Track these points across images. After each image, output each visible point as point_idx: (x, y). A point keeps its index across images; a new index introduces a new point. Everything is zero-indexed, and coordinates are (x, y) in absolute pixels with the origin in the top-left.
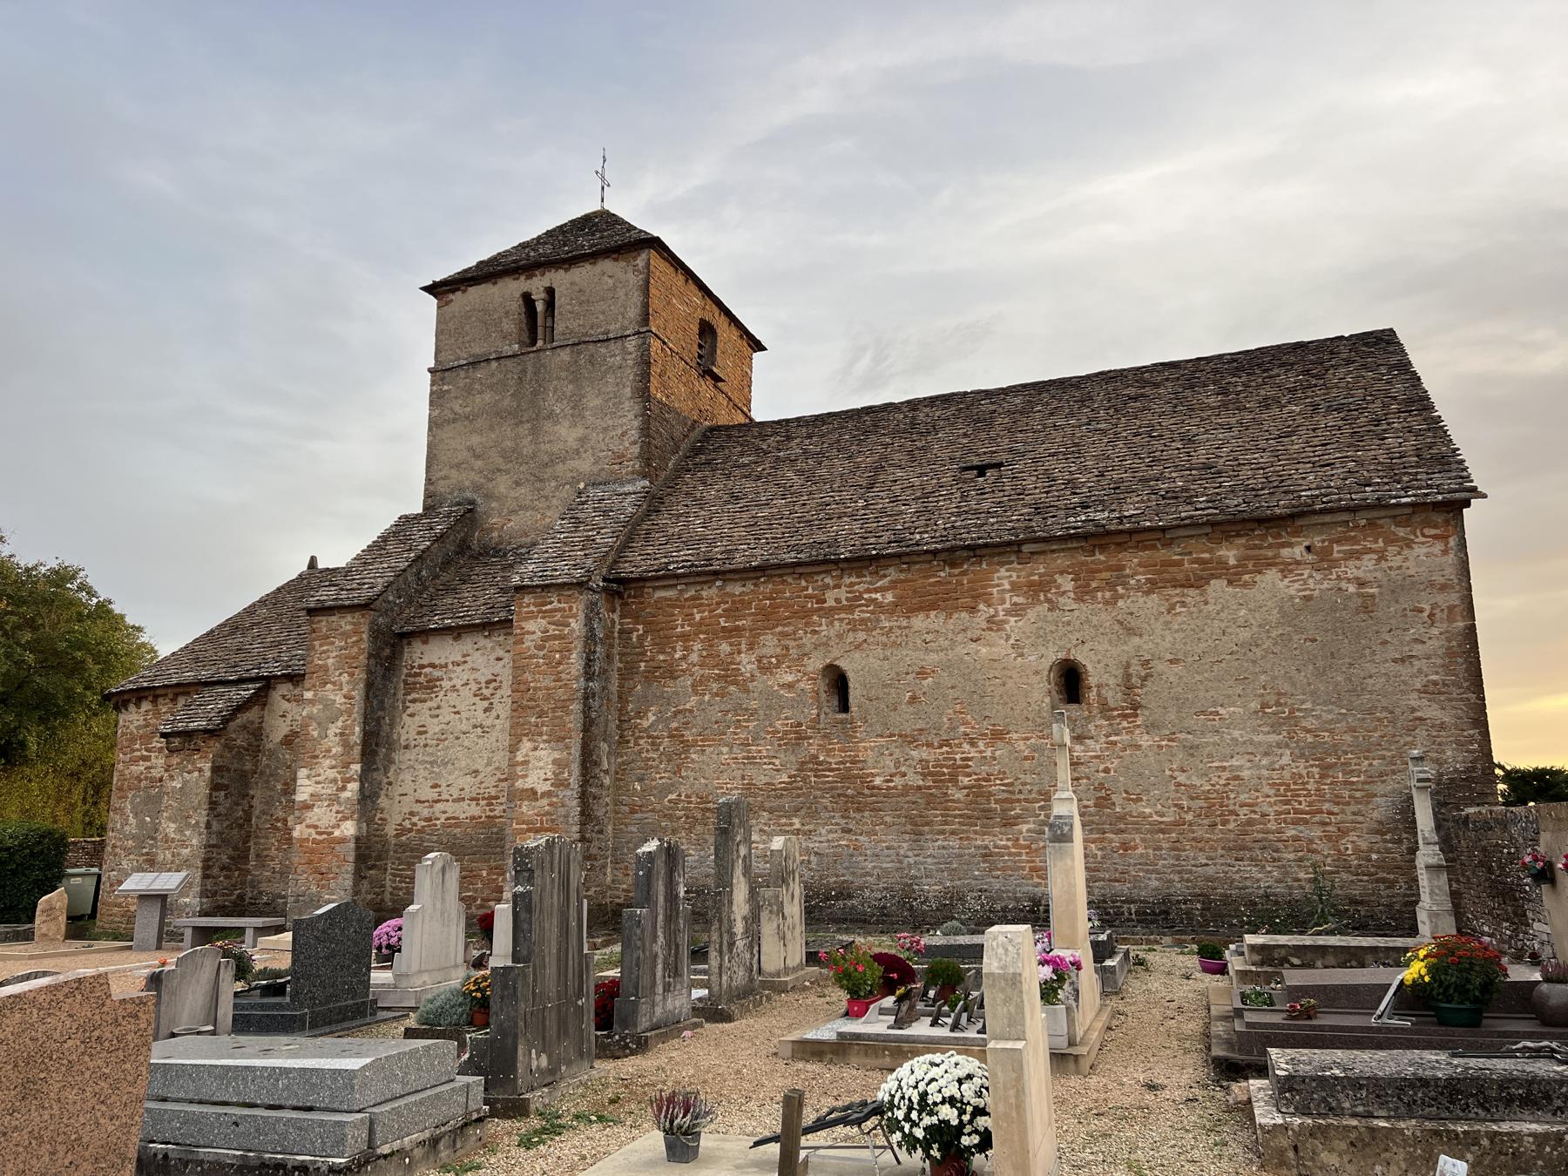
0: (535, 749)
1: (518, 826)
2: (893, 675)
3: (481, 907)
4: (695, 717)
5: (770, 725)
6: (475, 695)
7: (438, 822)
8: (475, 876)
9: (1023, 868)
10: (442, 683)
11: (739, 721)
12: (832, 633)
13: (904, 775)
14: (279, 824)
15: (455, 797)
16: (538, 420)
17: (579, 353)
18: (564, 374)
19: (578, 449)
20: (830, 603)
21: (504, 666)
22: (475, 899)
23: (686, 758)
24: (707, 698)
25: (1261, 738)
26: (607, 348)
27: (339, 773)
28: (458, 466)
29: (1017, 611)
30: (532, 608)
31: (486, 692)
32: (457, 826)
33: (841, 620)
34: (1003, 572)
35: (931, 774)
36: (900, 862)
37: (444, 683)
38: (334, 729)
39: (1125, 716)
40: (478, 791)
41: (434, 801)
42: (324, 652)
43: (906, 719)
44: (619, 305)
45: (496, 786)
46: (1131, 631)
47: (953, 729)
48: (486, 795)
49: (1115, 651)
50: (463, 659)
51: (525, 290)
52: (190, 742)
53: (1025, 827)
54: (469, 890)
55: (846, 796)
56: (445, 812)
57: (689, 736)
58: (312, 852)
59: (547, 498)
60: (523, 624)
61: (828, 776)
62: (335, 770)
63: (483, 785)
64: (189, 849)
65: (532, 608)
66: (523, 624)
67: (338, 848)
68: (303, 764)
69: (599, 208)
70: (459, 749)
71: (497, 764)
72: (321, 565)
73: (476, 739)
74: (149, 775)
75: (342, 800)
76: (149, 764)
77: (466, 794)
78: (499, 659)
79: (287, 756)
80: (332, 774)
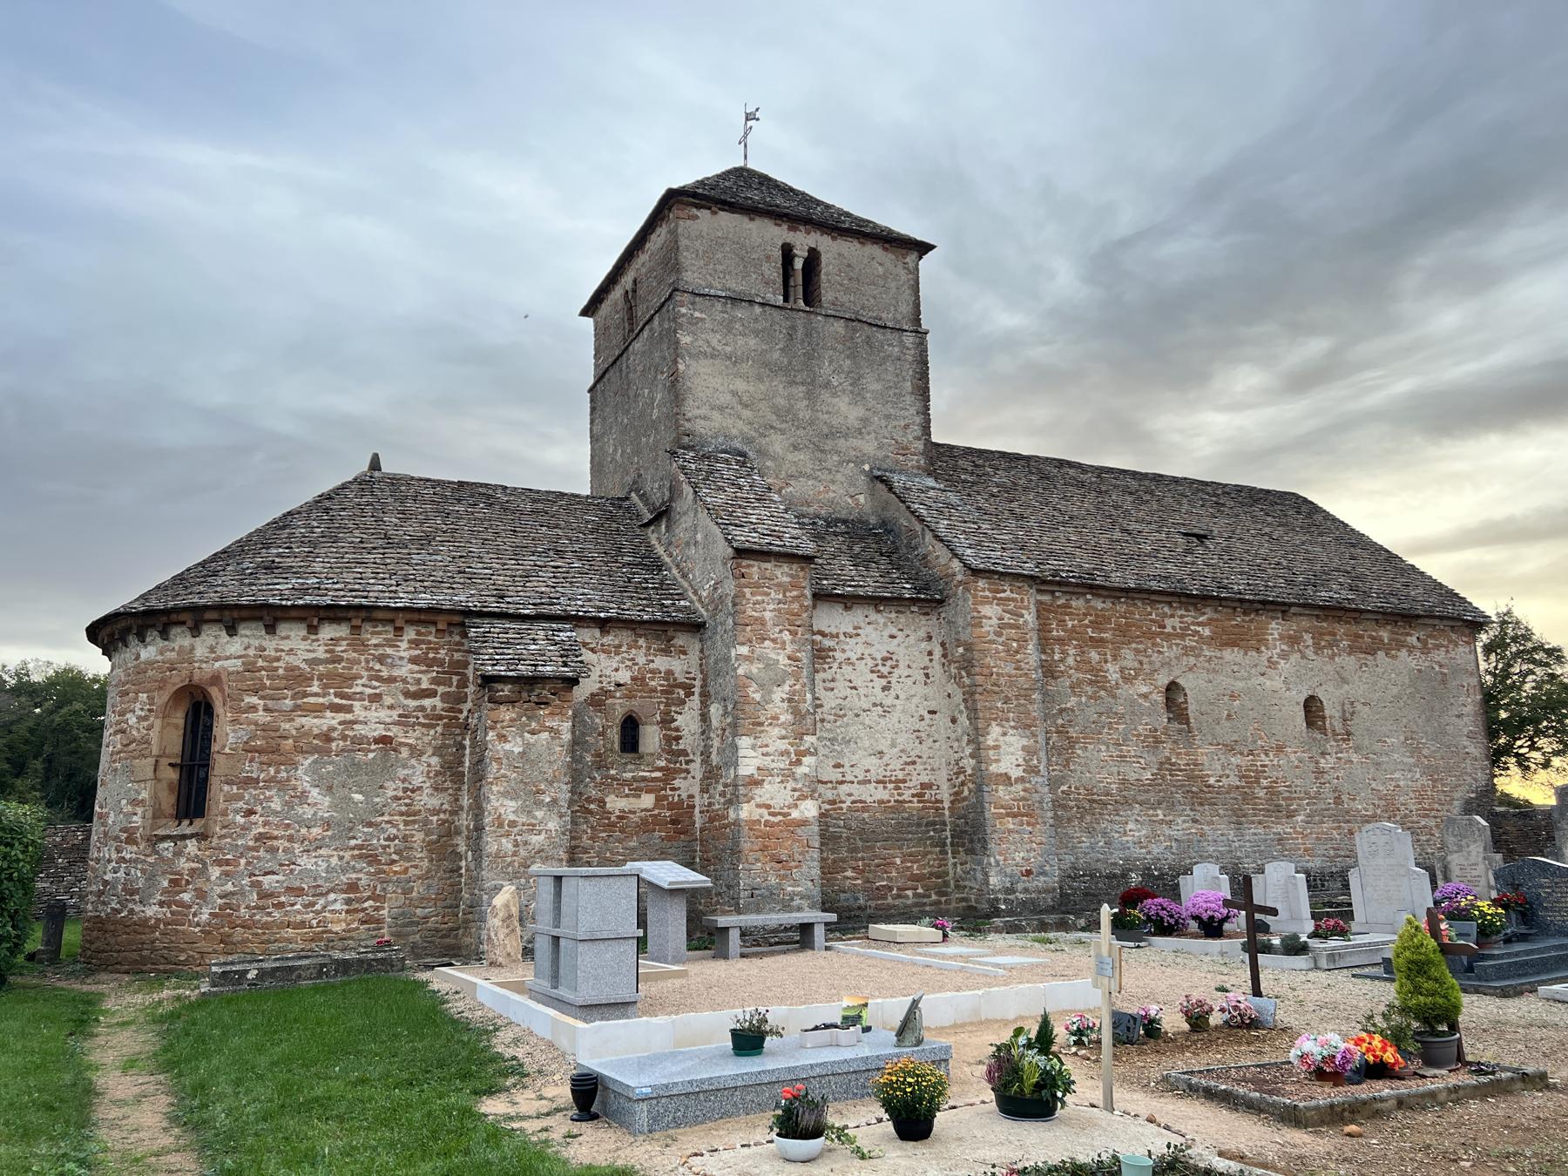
0: (1005, 734)
1: (997, 811)
2: (1215, 696)
3: (899, 896)
4: (1076, 716)
5: (1135, 729)
6: (872, 672)
7: (844, 806)
8: (888, 864)
9: (1300, 849)
10: (835, 654)
11: (1111, 723)
12: (1172, 655)
13: (1228, 776)
14: (592, 806)
15: (860, 778)
16: (814, 387)
17: (855, 330)
18: (840, 347)
19: (860, 429)
20: (1169, 630)
21: (899, 645)
22: (891, 889)
23: (1073, 753)
24: (1084, 699)
25: (1405, 760)
26: (884, 334)
27: (791, 744)
28: (721, 409)
29: (1284, 656)
30: (987, 593)
31: (885, 670)
32: (864, 810)
33: (1177, 645)
34: (1273, 625)
35: (1244, 776)
36: (1230, 846)
37: (838, 655)
38: (779, 694)
39: (1344, 740)
40: (885, 773)
41: (837, 782)
42: (757, 603)
43: (1225, 732)
44: (890, 296)
45: (903, 770)
46: (1344, 681)
47: (1255, 742)
48: (893, 779)
49: (1337, 693)
50: (855, 632)
51: (788, 241)
52: (530, 691)
53: (1299, 818)
54: (883, 880)
55: (1192, 792)
56: (850, 795)
57: (1073, 733)
58: (768, 836)
59: (830, 471)
60: (980, 608)
61: (1178, 775)
62: (786, 741)
63: (889, 768)
64: (542, 837)
65: (987, 593)
66: (980, 608)
67: (799, 831)
68: (745, 731)
69: (742, 165)
70: (861, 727)
71: (902, 747)
72: (388, 467)
73: (877, 718)
74: (351, 733)
75: (798, 776)
76: (349, 717)
77: (872, 776)
78: (893, 637)
79: (597, 720)
80: (783, 745)
